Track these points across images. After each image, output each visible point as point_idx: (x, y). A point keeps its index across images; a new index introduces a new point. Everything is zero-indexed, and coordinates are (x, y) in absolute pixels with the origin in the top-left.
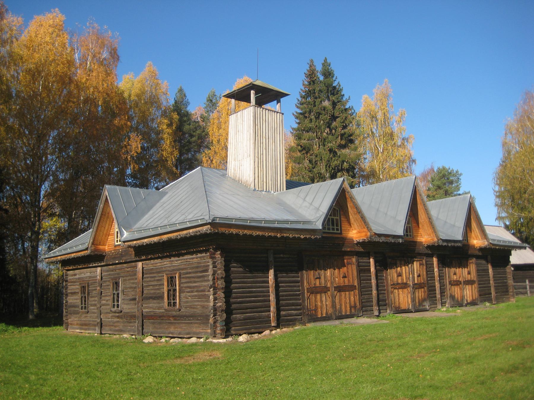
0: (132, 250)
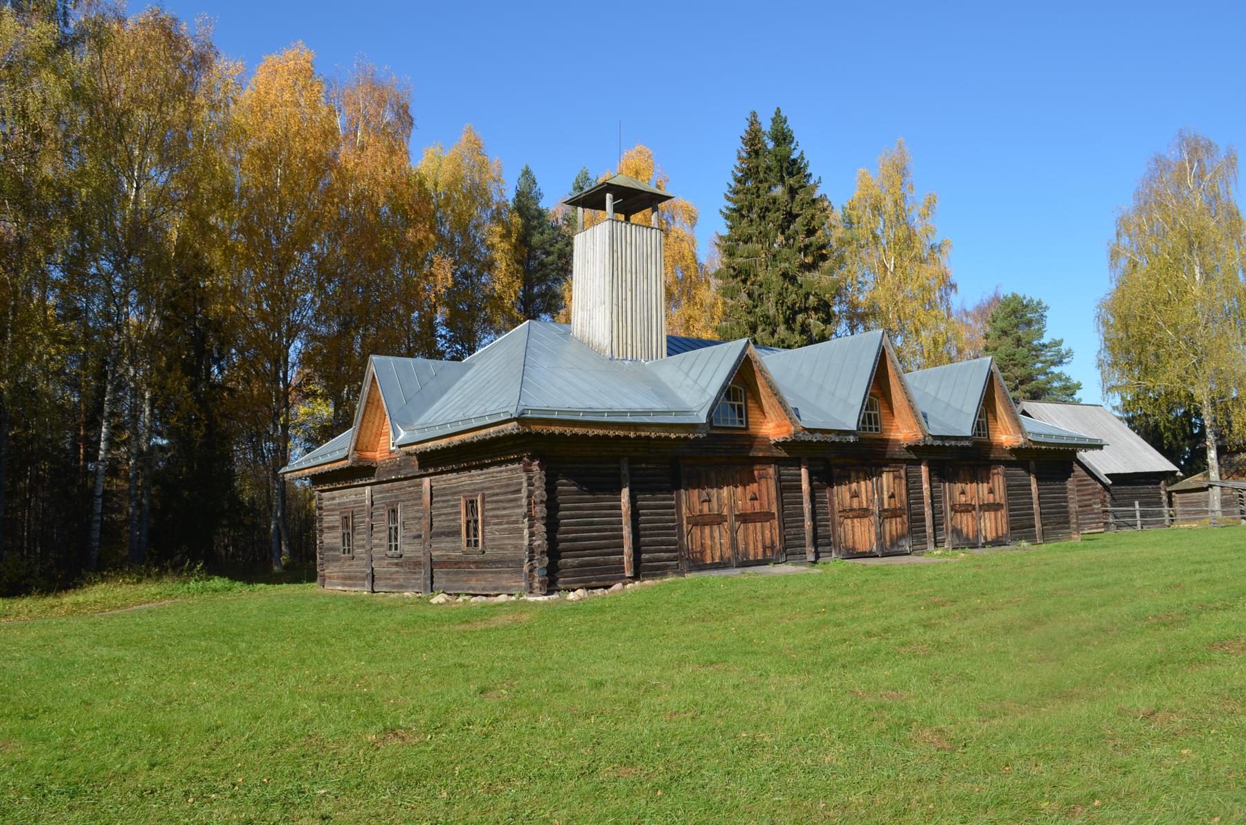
0: (415, 458)
